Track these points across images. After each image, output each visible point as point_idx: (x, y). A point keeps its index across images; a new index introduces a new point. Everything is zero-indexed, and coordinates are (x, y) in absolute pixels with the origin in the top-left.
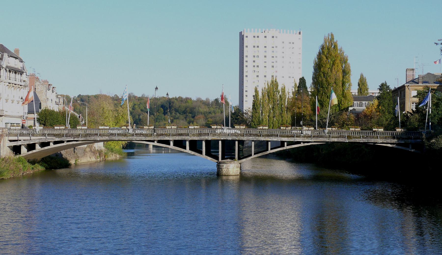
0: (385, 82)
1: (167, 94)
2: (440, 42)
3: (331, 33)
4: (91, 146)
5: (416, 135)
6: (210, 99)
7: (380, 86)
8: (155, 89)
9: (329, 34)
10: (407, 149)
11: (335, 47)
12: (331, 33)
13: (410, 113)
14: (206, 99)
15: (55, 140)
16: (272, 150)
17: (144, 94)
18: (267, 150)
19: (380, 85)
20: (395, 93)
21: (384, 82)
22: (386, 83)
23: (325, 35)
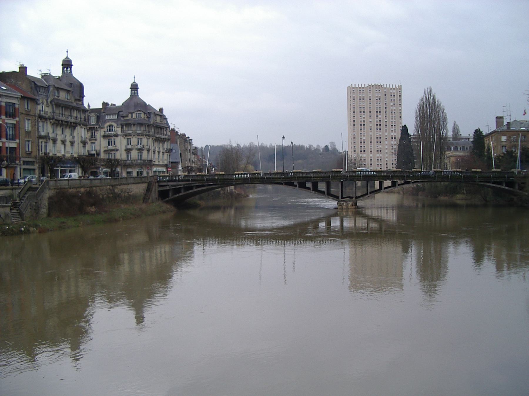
0: (479, 128)
1: (292, 143)
2: (527, 93)
3: (430, 87)
4: (225, 189)
5: (485, 174)
6: (321, 146)
7: (474, 132)
8: (282, 138)
9: (428, 88)
10: (502, 187)
11: (434, 99)
12: (430, 87)
13: (502, 156)
14: (250, 144)
15: (386, 181)
16: (386, 190)
17: (262, 143)
18: (168, 197)
19: (474, 131)
20: (487, 138)
21: (477, 128)
22: (479, 130)
23: (525, 108)
